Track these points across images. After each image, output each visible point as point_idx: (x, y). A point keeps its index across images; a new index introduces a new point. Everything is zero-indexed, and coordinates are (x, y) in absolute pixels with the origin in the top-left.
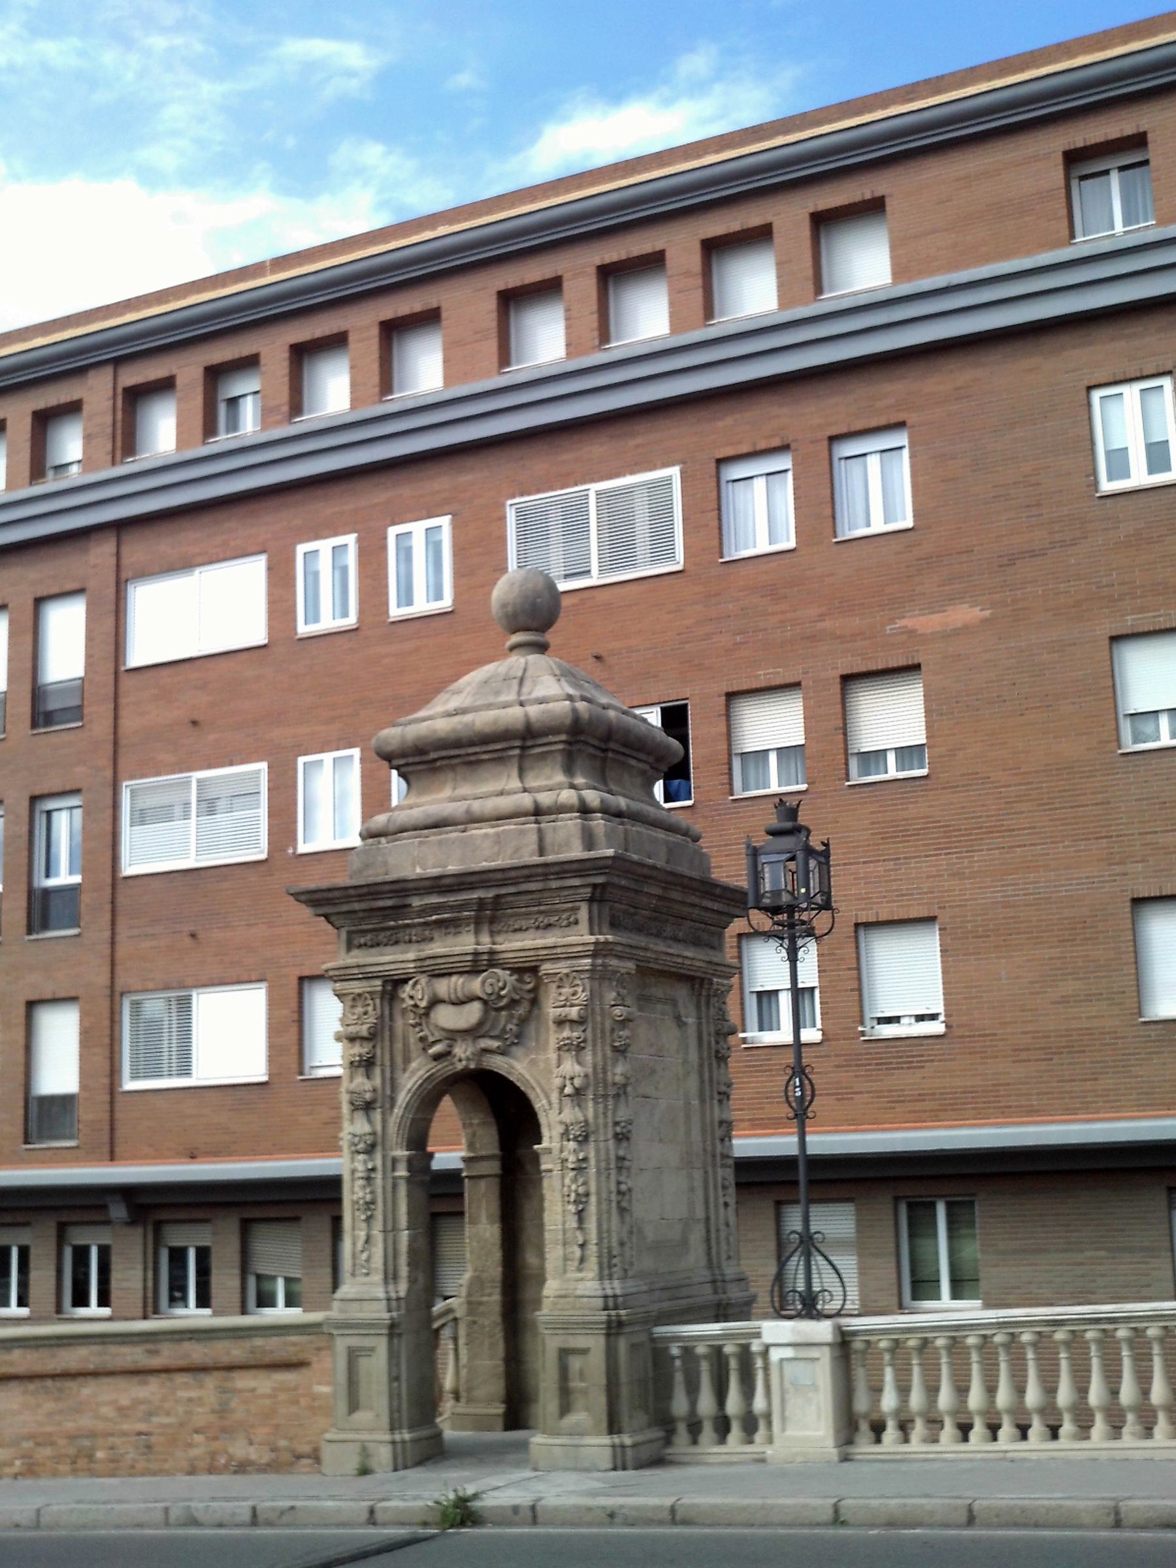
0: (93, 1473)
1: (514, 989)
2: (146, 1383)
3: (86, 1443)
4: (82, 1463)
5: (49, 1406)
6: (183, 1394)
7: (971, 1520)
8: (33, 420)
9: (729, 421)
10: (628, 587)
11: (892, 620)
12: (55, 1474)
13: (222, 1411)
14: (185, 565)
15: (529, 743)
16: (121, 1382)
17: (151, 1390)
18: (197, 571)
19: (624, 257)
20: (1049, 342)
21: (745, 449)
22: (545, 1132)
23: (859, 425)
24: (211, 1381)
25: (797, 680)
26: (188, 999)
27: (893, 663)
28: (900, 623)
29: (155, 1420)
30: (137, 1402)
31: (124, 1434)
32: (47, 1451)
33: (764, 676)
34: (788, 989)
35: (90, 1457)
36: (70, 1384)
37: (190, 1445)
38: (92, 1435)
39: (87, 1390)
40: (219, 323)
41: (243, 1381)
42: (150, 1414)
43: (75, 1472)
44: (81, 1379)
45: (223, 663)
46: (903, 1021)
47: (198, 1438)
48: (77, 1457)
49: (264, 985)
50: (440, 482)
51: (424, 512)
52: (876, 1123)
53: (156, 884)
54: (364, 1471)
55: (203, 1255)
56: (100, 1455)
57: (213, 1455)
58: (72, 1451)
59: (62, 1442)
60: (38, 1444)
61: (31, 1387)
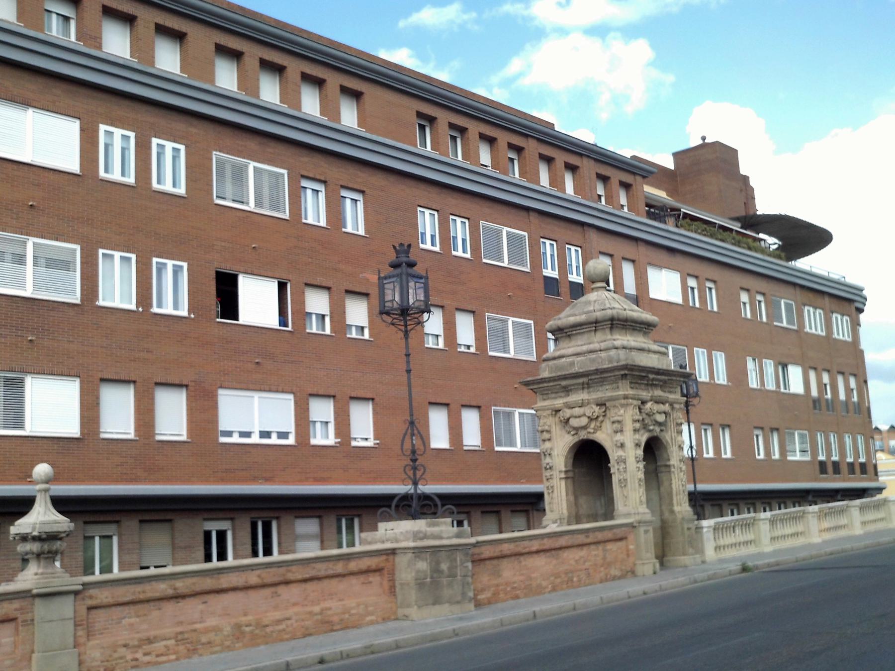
0: (574, 587)
1: (598, 412)
2: (582, 550)
3: (570, 575)
4: (570, 584)
5: (554, 562)
6: (594, 553)
7: (502, 625)
8: (320, 78)
9: (305, 159)
10: (264, 218)
11: (362, 273)
12: (562, 589)
13: (604, 558)
14: (26, 103)
15: (597, 325)
16: (575, 550)
17: (583, 553)
18: (30, 111)
19: (271, 60)
20: (477, 200)
21: (311, 175)
22: (611, 461)
23: (350, 185)
24: (600, 547)
25: (330, 286)
26: (20, 383)
27: (358, 290)
28: (364, 275)
29: (587, 564)
30: (581, 557)
31: (581, 570)
32: (559, 580)
33: (319, 281)
34: (71, 619)
35: (572, 581)
36: (560, 552)
37: (600, 572)
38: (572, 572)
39: (566, 554)
40: (277, 41)
41: (610, 546)
42: (585, 562)
43: (568, 587)
44: (526, 556)
45: (51, 176)
46: (357, 440)
47: (602, 569)
48: (568, 581)
49: (78, 381)
50: (197, 130)
51: (172, 138)
52: (356, 482)
53: (262, 273)
54: (655, 573)
55: (221, 535)
56: (575, 579)
57: (606, 575)
58: (566, 579)
59: (563, 576)
60: (556, 578)
61: (548, 554)
